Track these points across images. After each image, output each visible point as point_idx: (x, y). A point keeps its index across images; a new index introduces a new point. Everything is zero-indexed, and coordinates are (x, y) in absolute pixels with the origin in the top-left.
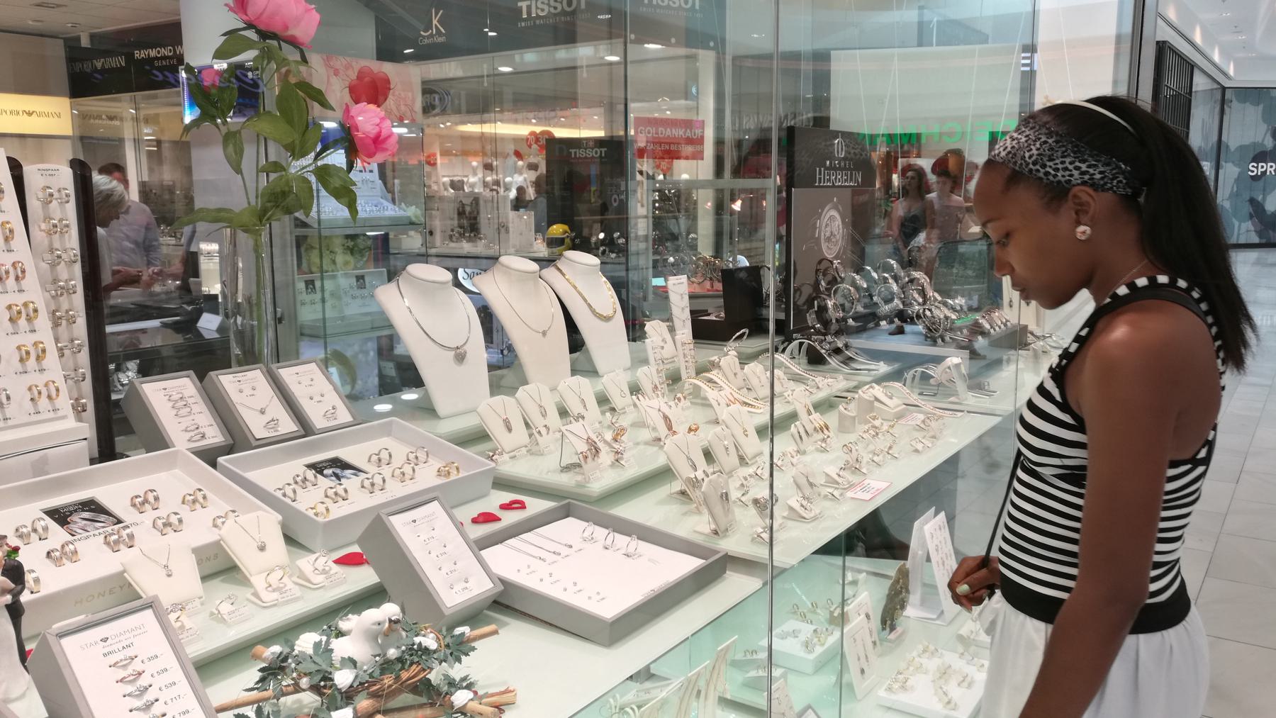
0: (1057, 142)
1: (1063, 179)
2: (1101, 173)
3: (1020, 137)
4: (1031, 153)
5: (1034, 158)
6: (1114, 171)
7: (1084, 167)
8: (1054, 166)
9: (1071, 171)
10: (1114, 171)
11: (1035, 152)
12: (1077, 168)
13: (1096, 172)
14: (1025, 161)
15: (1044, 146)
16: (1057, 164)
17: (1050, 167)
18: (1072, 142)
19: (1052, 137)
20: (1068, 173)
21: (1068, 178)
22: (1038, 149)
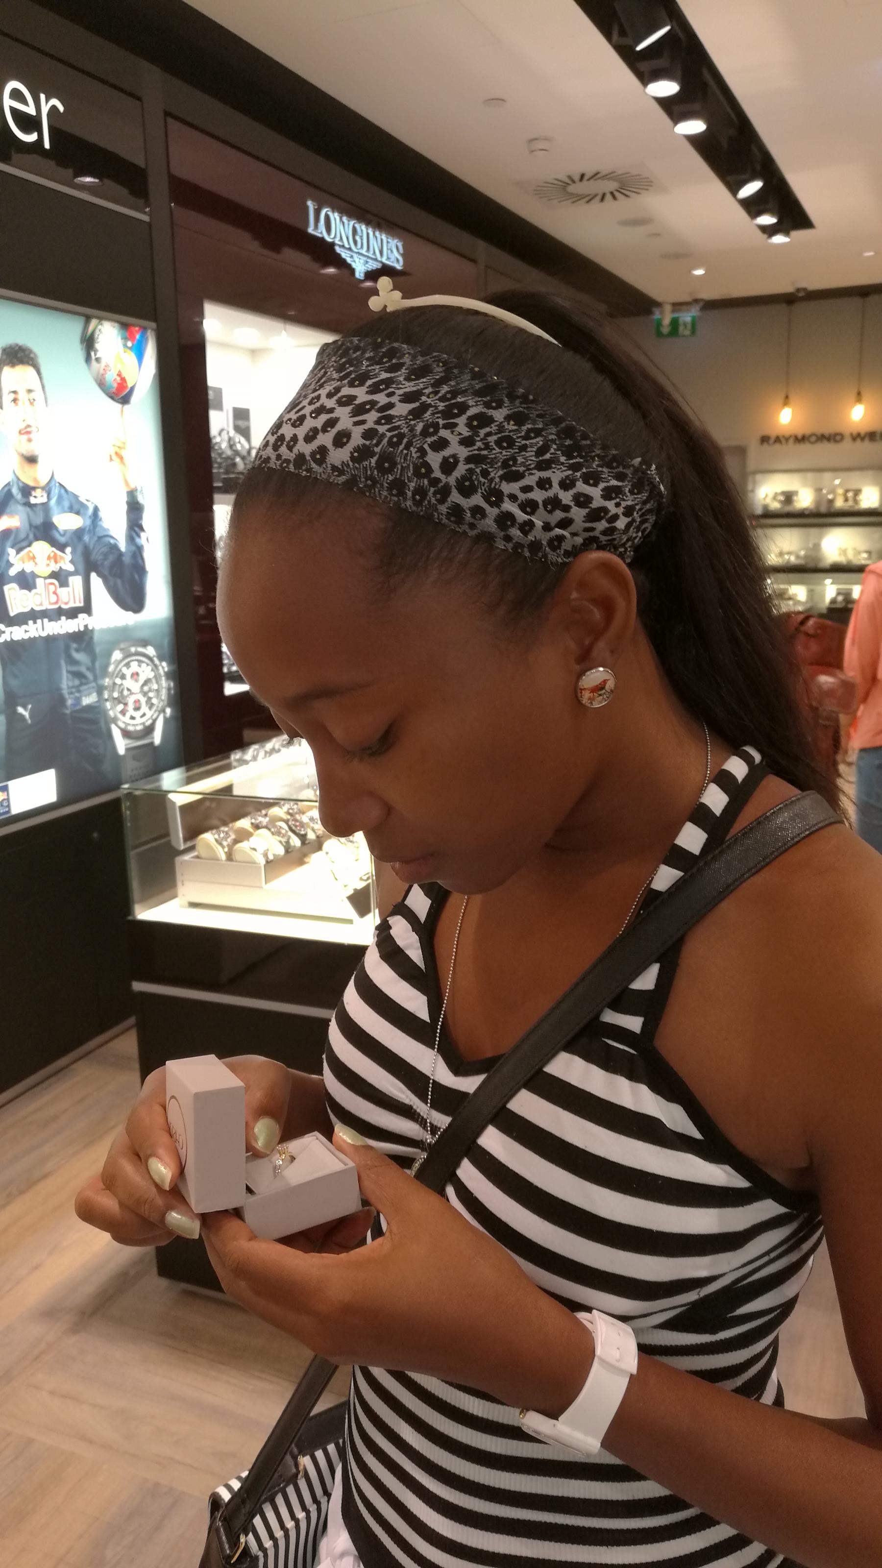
0: (518, 418)
1: (544, 538)
2: (407, 398)
3: (381, 399)
4: (447, 453)
5: (461, 469)
6: (445, 389)
7: (361, 394)
8: (522, 497)
9: (567, 508)
10: (445, 389)
11: (455, 448)
12: (582, 500)
13: (394, 399)
14: (435, 482)
15: (482, 432)
16: (527, 489)
17: (513, 498)
18: (556, 421)
19: (499, 406)
20: (559, 515)
21: (558, 531)
22: (466, 442)
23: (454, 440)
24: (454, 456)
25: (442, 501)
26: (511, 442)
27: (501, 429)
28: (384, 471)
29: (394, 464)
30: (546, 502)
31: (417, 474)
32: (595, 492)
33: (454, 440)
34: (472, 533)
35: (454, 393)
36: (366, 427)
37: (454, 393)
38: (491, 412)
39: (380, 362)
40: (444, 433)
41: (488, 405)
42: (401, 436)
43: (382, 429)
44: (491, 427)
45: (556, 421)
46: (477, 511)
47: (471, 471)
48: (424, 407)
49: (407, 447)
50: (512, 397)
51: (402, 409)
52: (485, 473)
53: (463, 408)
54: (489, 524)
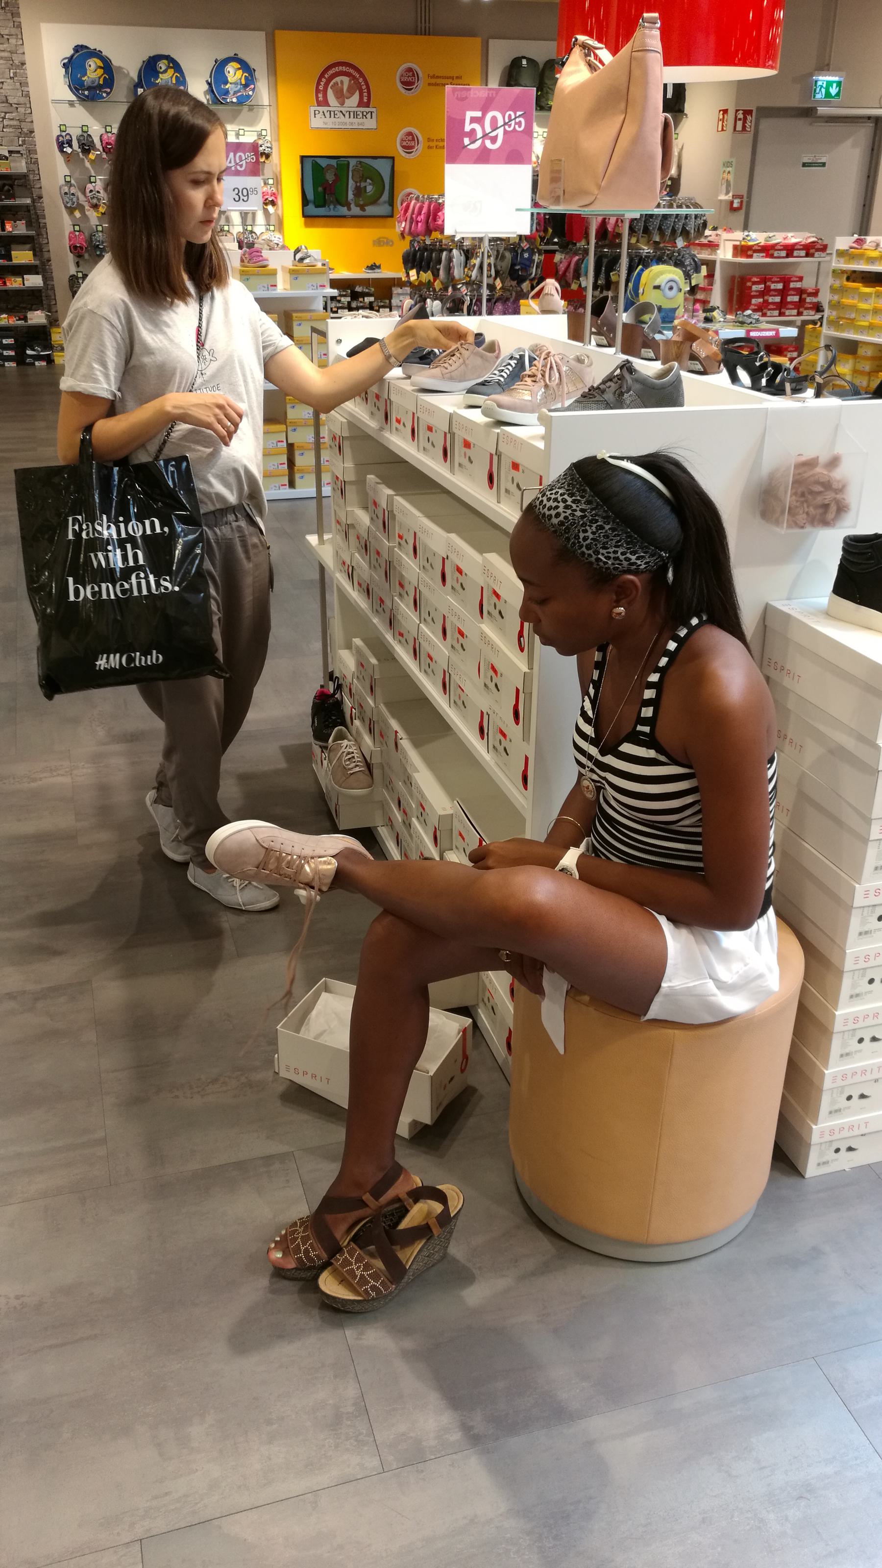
2: (582, 510)
5: (589, 541)
6: (594, 512)
8: (606, 555)
10: (594, 512)
11: (589, 534)
18: (627, 533)
19: (608, 524)
22: (593, 533)
23: (590, 531)
24: (588, 537)
25: (580, 549)
26: (608, 537)
27: (606, 532)
28: (566, 533)
29: (569, 532)
30: (614, 558)
31: (575, 537)
32: (633, 558)
33: (590, 531)
34: (586, 561)
35: (596, 515)
36: (566, 514)
37: (596, 515)
38: (605, 526)
39: (579, 492)
40: (588, 528)
41: (605, 523)
42: (575, 523)
43: (570, 518)
44: (305, 1240)
45: (627, 533)
46: (590, 555)
47: (591, 543)
48: (585, 516)
49: (575, 527)
50: (614, 522)
51: (578, 513)
52: (596, 545)
53: (597, 521)
54: (593, 559)
